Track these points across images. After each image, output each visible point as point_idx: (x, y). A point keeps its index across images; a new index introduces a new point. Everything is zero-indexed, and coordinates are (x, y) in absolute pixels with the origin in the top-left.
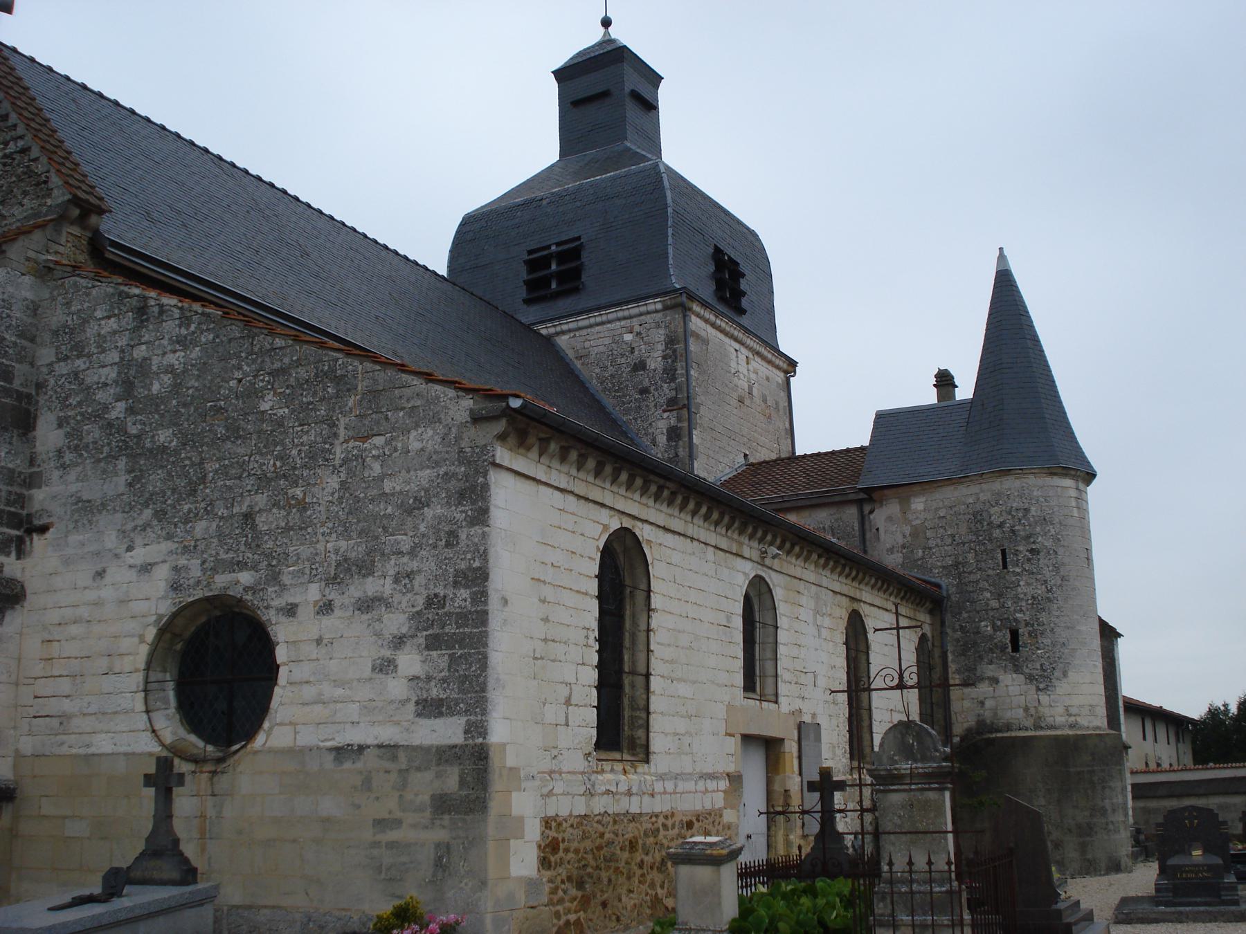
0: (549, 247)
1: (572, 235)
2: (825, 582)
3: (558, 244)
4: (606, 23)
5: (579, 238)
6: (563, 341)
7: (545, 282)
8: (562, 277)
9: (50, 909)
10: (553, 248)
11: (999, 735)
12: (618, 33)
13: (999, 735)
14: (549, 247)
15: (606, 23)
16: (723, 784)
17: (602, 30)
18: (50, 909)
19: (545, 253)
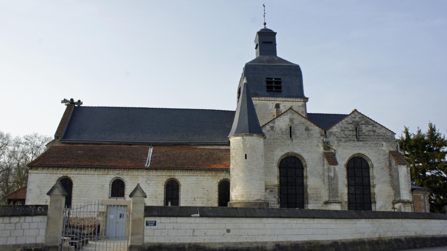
0: (272, 79)
1: (279, 78)
2: (163, 174)
3: (275, 79)
4: (265, 24)
5: (280, 79)
6: (253, 101)
7: (272, 87)
8: (276, 88)
9: (246, 155)
10: (274, 79)
11: (130, 231)
12: (268, 27)
13: (130, 231)
14: (272, 79)
15: (265, 24)
16: (185, 201)
17: (264, 26)
18: (246, 155)
19: (270, 80)
